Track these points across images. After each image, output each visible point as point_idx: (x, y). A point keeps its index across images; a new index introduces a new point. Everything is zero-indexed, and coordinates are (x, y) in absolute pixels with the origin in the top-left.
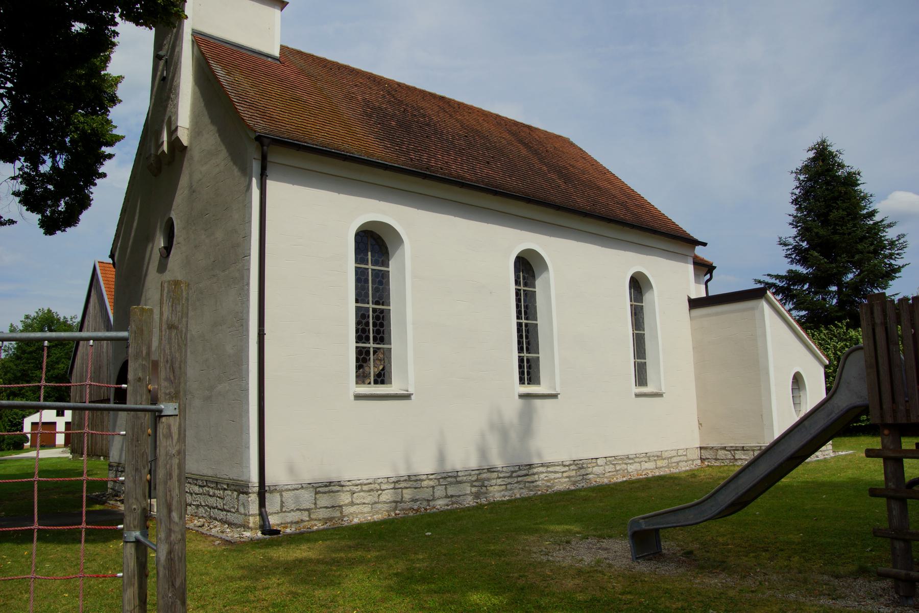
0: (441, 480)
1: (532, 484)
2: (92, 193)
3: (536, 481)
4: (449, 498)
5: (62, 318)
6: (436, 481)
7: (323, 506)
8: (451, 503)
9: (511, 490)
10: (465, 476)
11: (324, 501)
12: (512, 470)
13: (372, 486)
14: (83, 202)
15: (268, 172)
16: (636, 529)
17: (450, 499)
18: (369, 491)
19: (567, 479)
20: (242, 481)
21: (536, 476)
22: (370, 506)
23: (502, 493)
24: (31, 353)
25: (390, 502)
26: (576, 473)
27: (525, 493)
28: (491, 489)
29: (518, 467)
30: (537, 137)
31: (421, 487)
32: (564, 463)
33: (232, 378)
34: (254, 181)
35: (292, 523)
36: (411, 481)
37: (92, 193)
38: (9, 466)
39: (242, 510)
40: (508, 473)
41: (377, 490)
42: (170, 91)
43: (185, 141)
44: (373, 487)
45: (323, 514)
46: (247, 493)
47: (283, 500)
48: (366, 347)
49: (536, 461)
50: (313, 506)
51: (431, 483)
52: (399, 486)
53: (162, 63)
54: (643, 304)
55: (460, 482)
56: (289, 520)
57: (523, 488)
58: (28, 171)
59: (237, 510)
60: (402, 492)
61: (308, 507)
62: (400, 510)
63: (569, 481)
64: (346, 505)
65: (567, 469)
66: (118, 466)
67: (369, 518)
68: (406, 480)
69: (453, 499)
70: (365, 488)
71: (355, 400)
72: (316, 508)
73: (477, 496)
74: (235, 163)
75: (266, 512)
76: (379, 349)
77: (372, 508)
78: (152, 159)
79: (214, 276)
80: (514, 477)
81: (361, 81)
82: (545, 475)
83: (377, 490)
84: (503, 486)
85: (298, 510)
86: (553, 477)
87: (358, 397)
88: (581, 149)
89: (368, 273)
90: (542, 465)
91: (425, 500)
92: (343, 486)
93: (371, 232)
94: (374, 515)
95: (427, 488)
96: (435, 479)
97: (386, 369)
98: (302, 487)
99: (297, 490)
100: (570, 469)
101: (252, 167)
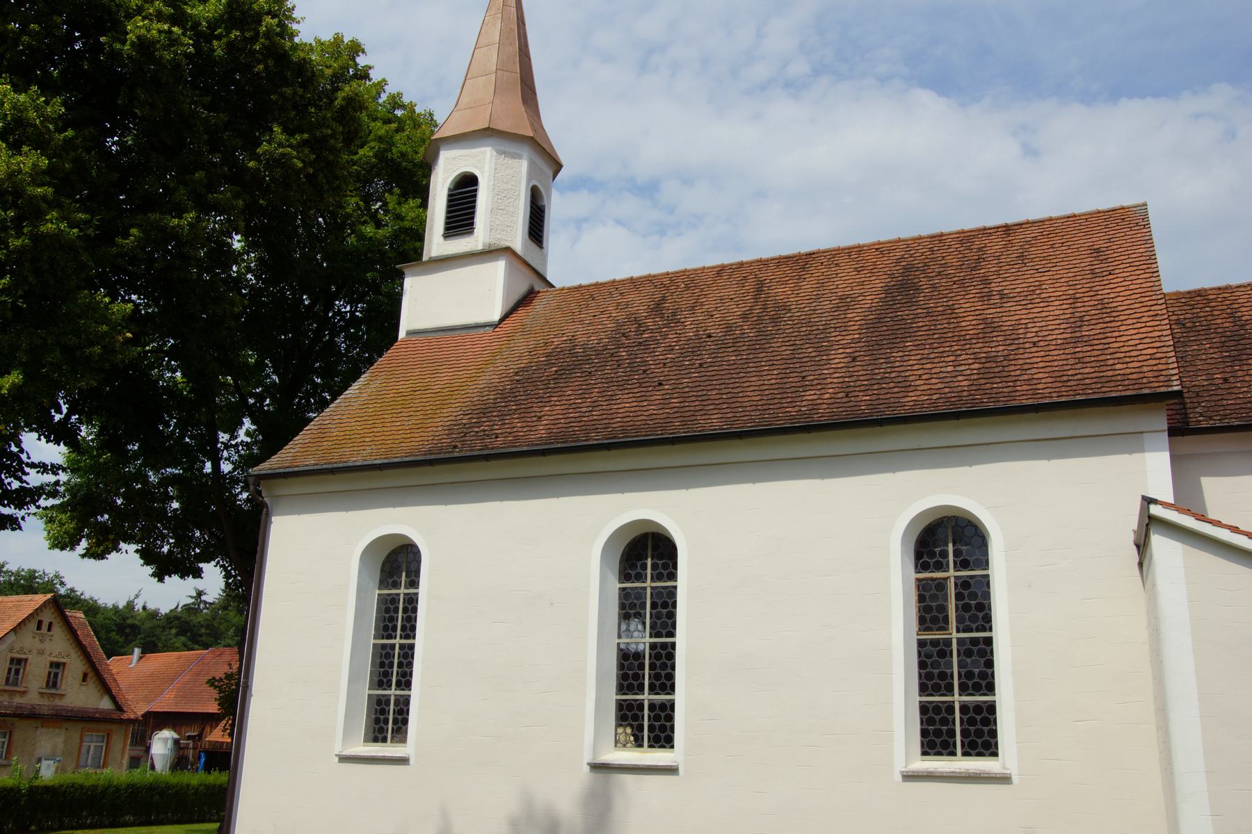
48: (385, 695)
54: (377, 592)
71: (339, 762)
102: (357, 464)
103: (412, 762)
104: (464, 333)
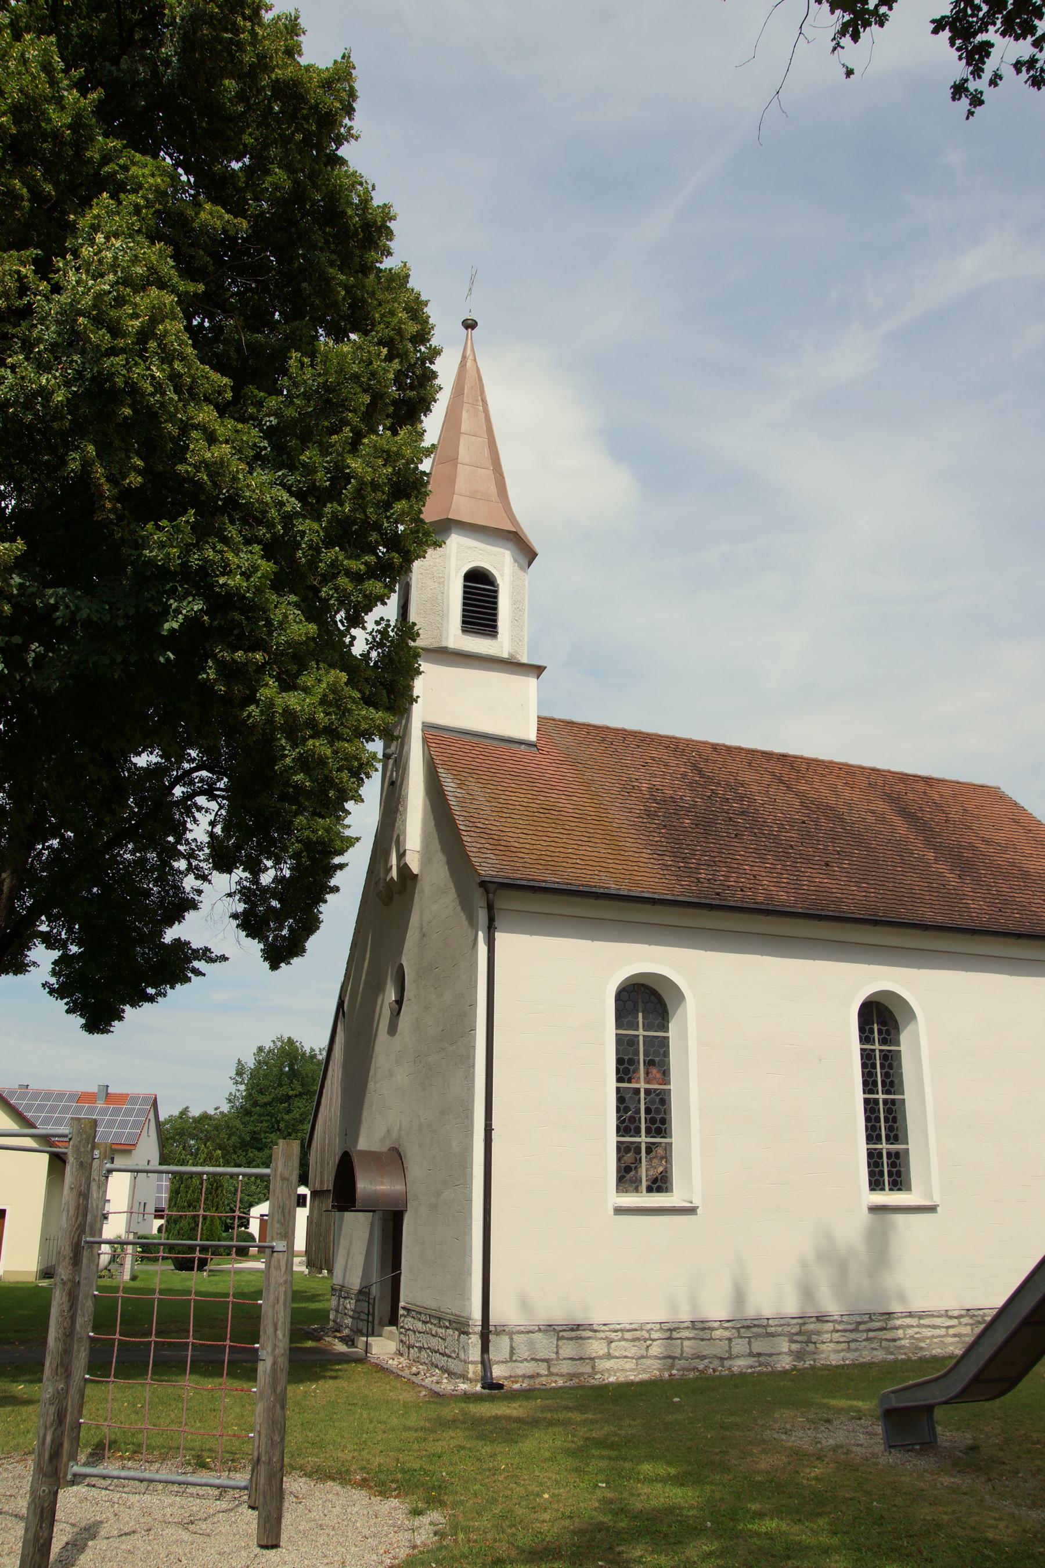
0: (742, 1330)
1: (892, 1344)
2: (321, 913)
3: (900, 1339)
4: (754, 1356)
5: (308, 1051)
6: (734, 1331)
7: (566, 1356)
8: (757, 1364)
9: (856, 1350)
10: (781, 1325)
11: (568, 1350)
12: (858, 1320)
13: (638, 1334)
14: (309, 925)
15: (496, 924)
16: (887, 1406)
17: (756, 1359)
18: (634, 1340)
19: (957, 1339)
20: (464, 1317)
21: (900, 1332)
22: (634, 1361)
23: (842, 1354)
24: (266, 1104)
25: (665, 1358)
26: (972, 1329)
27: (880, 1355)
28: (823, 1347)
29: (868, 1316)
30: (936, 797)
31: (711, 1339)
32: (950, 1313)
33: (457, 1183)
34: (481, 935)
35: (524, 1376)
36: (696, 1329)
37: (321, 913)
38: (224, 1281)
39: (462, 1356)
40: (850, 1324)
41: (645, 1340)
42: (398, 802)
43: (415, 869)
44: (637, 1334)
45: (566, 1367)
46: (467, 1333)
47: (514, 1345)
49: (896, 1307)
50: (554, 1356)
51: (727, 1334)
52: (678, 1336)
53: (391, 762)
55: (773, 1335)
56: (520, 1372)
57: (876, 1349)
58: (248, 884)
59: (458, 1356)
60: (682, 1343)
61: (547, 1357)
62: (678, 1370)
63: (958, 1342)
64: (600, 1358)
65: (954, 1322)
66: (341, 1290)
67: (632, 1378)
68: (688, 1328)
69: (761, 1359)
70: (628, 1335)
72: (558, 1359)
73: (799, 1355)
74: (463, 909)
75: (489, 1360)
76: (653, 1143)
77: (637, 1365)
78: (381, 885)
79: (443, 1049)
80: (863, 1331)
81: (654, 753)
82: (917, 1330)
83: (645, 1340)
84: (844, 1344)
85: (533, 1359)
86: (929, 1334)
87: (619, 1211)
88: (1016, 804)
89: (638, 1041)
90: (910, 1315)
91: (717, 1358)
92: (596, 1331)
93: (643, 985)
94: (639, 1374)
95: (720, 1340)
96: (733, 1328)
97: (668, 1170)
98: (540, 1330)
99: (533, 1333)
100: (960, 1323)
101: (477, 916)
102: (621, 893)
103: (699, 1211)
104: (495, 743)
